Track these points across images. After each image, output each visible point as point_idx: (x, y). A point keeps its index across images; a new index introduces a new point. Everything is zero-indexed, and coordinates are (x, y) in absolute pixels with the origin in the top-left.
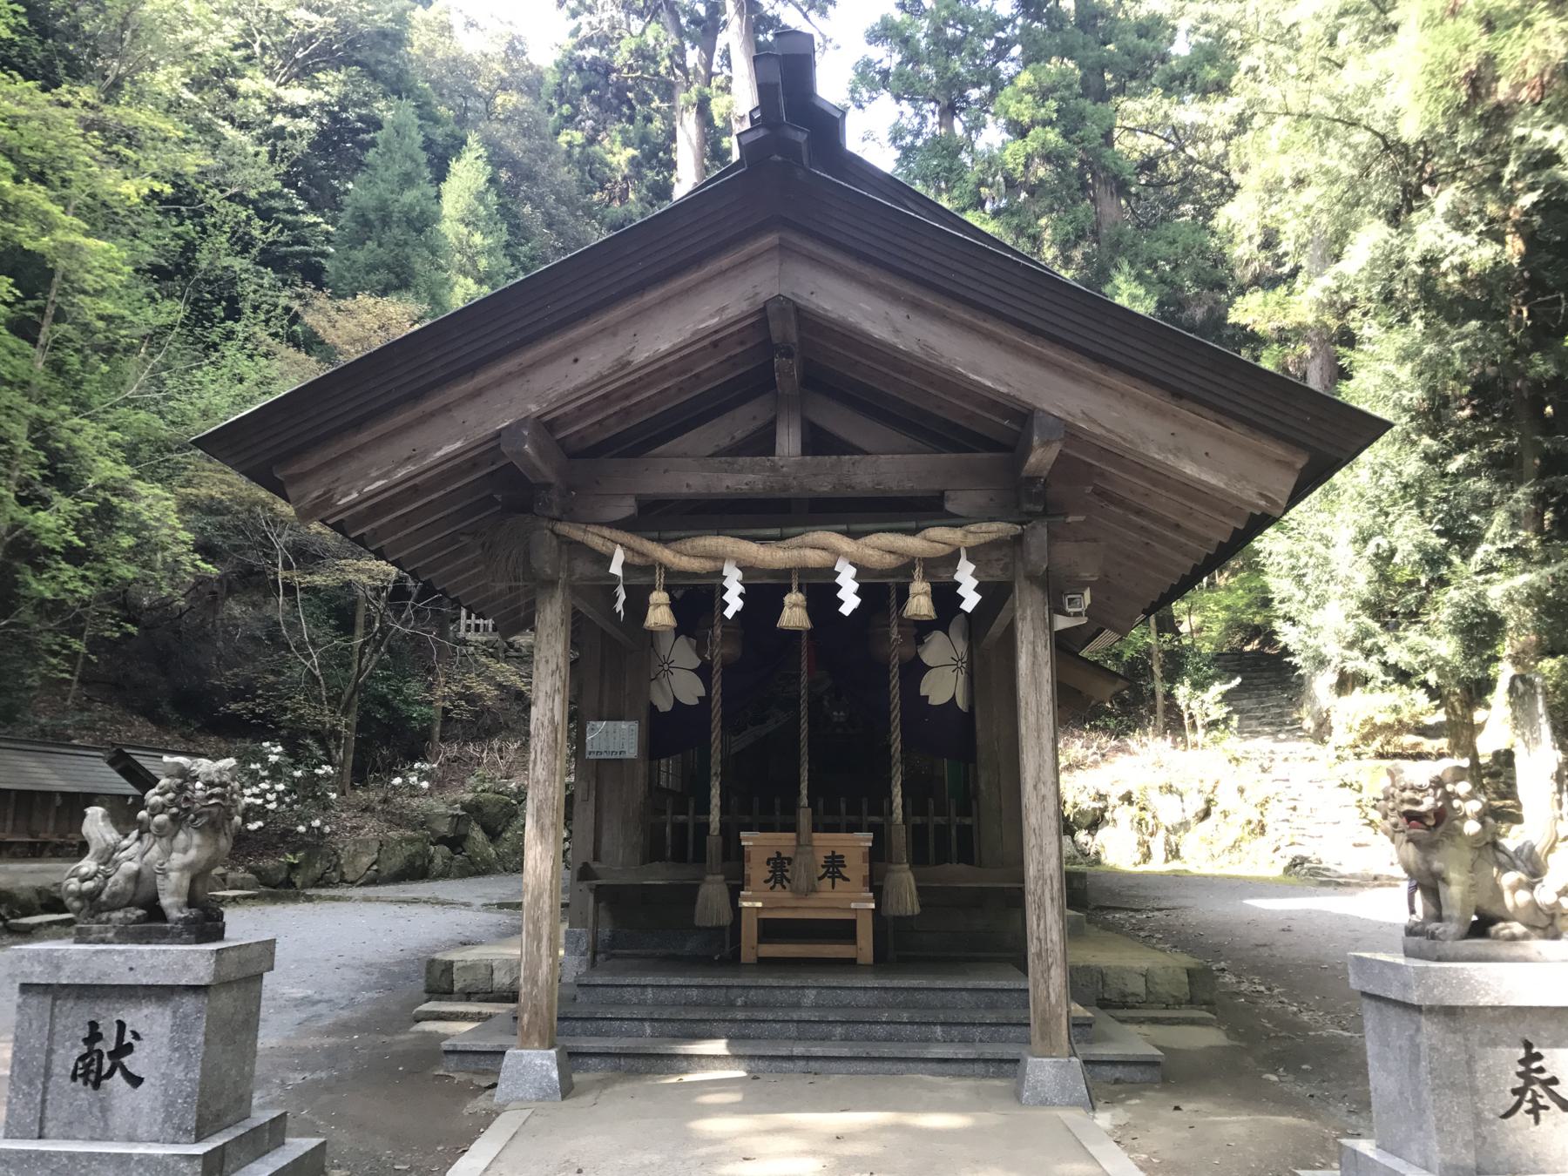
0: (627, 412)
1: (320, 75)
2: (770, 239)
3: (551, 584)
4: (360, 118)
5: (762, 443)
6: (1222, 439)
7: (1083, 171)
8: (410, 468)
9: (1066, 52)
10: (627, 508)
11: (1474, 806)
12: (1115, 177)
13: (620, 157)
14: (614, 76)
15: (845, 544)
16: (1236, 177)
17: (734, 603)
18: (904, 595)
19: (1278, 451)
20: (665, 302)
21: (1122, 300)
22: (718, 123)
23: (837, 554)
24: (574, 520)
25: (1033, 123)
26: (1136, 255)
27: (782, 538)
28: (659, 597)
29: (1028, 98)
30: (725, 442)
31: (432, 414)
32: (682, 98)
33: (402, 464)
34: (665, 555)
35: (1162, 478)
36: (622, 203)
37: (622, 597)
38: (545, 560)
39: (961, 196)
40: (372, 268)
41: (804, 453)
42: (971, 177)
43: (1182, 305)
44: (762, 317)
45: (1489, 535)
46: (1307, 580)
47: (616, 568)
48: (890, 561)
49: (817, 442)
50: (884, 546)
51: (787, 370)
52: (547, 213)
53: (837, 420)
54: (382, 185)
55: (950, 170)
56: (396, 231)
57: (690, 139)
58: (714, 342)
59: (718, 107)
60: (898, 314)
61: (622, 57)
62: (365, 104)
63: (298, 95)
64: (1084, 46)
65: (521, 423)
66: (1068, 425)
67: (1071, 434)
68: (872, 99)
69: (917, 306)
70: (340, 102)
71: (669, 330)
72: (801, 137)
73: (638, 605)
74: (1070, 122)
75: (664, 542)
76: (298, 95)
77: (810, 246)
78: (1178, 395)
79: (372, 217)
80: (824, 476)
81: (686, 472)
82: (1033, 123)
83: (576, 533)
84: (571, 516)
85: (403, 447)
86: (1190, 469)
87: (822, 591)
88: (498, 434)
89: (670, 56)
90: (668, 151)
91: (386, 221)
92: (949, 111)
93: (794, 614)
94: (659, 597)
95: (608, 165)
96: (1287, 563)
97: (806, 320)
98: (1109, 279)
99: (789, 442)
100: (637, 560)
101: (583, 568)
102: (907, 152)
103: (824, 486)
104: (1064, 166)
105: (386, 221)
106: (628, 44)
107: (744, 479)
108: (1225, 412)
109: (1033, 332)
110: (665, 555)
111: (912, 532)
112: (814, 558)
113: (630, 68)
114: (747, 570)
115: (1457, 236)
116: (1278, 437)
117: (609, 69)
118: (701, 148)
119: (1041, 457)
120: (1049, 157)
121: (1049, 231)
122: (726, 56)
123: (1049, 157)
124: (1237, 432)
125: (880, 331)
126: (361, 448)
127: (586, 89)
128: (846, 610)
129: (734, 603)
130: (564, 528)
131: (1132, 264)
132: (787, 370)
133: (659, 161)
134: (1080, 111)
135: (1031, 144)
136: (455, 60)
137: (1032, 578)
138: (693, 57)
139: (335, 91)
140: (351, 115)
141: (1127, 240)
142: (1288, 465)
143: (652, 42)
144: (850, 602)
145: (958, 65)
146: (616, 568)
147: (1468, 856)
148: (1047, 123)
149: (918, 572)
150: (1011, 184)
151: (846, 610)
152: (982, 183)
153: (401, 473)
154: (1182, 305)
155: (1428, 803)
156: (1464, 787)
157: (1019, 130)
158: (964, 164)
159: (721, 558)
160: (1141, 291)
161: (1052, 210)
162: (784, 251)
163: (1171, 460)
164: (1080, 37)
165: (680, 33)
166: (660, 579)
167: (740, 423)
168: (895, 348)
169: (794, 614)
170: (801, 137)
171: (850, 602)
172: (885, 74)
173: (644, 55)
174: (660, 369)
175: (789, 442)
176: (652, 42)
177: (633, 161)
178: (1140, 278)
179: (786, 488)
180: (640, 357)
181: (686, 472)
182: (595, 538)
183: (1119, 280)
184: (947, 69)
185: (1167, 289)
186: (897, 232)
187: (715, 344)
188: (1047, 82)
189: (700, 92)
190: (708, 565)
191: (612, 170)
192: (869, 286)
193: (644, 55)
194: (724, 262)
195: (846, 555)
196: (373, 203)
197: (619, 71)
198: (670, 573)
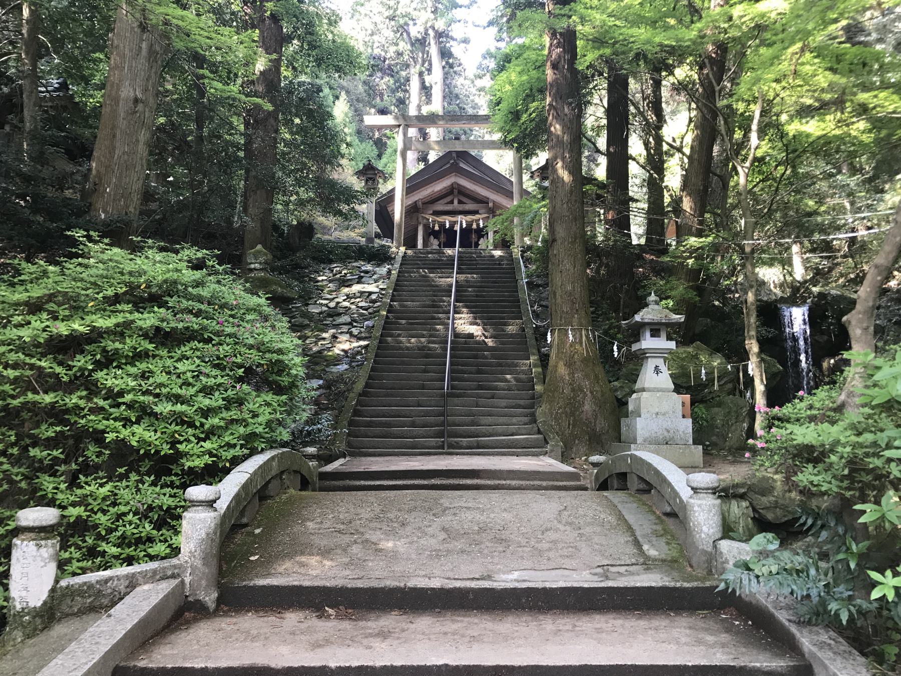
5: (452, 202)
17: (447, 226)
38: (420, 219)
49: (460, 202)
50: (470, 218)
51: (456, 191)
53: (464, 199)
67: (494, 202)
71: (440, 186)
73: (434, 227)
75: (268, 575)
80: (461, 207)
81: (440, 207)
99: (456, 202)
103: (461, 209)
107: (449, 208)
119: (491, 205)
121: (688, 61)
129: (447, 226)
132: (456, 191)
167: (449, 199)
175: (456, 202)
179: (810, 632)
180: (436, 190)
181: (440, 207)
182: (427, 216)
196: (818, 444)
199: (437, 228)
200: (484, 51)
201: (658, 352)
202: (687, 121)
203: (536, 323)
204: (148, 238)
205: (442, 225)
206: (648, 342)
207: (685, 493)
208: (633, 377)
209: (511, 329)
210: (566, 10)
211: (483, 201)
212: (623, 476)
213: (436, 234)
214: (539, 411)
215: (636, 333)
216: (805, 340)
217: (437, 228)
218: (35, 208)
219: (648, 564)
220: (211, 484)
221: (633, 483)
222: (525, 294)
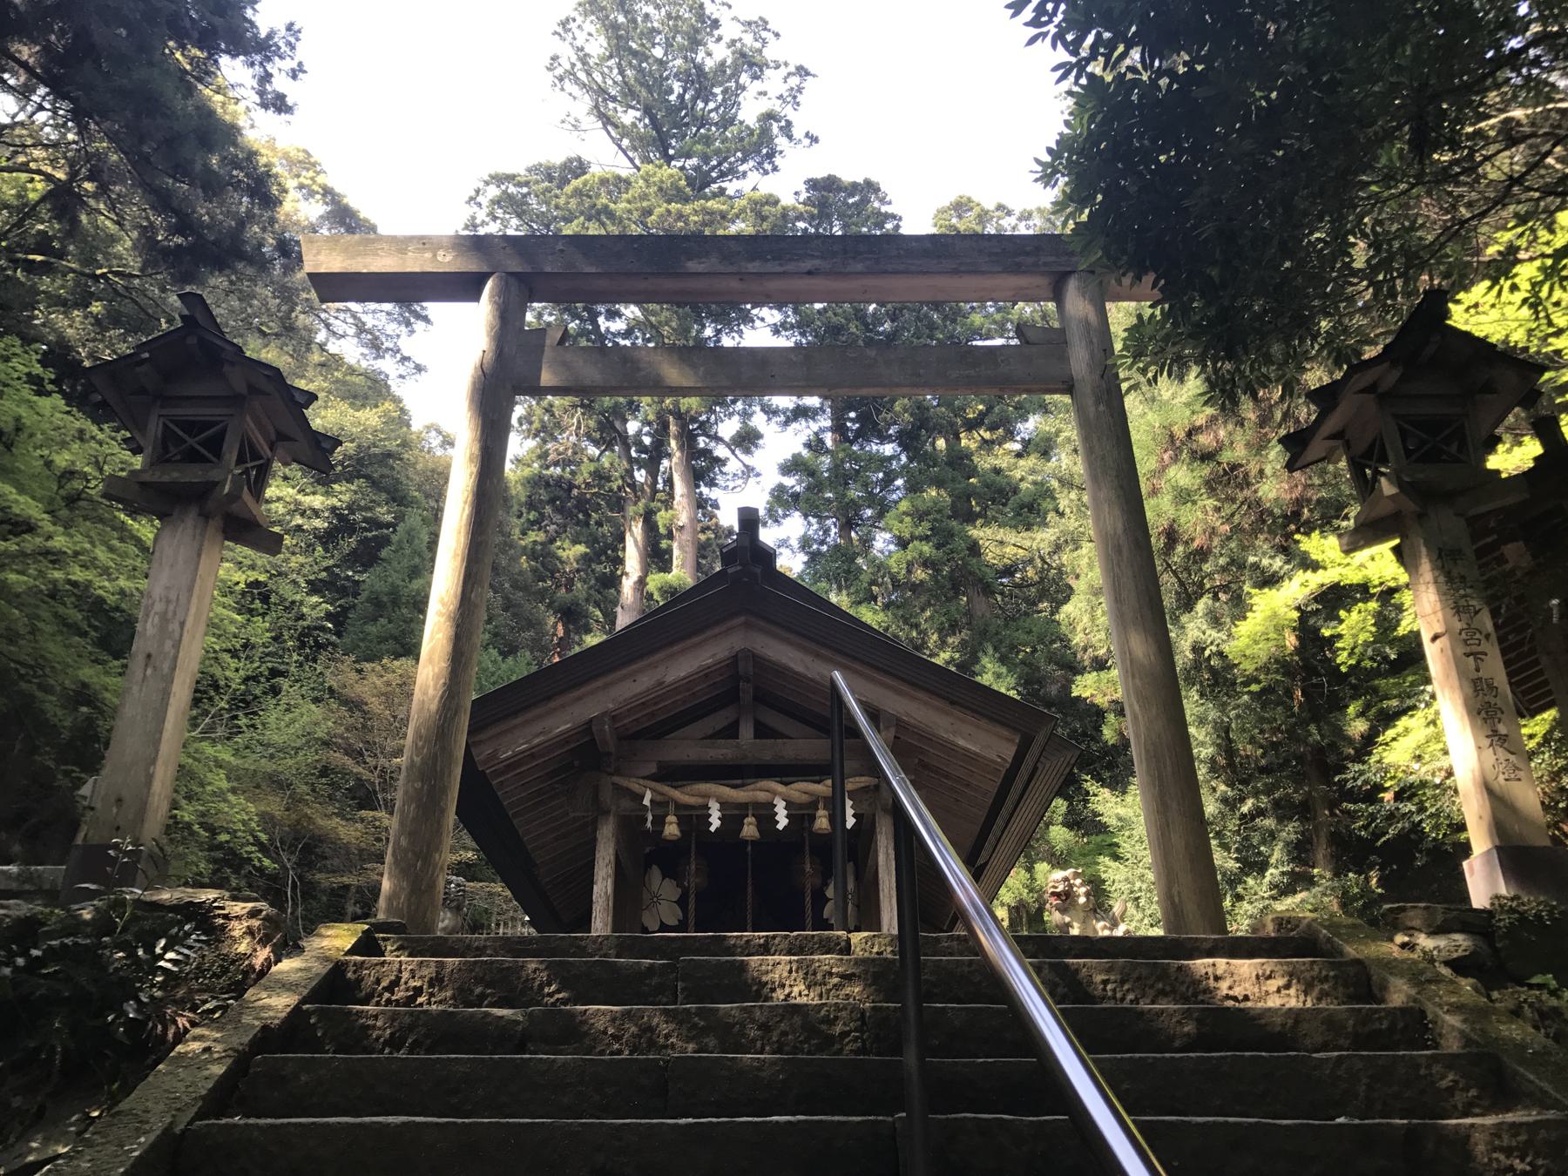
0: (653, 714)
1: (336, 487)
2: (742, 619)
3: (607, 813)
4: (365, 520)
5: (731, 732)
6: (978, 727)
7: (959, 578)
8: (542, 738)
9: (939, 483)
10: (652, 769)
11: (1083, 890)
12: (981, 580)
13: (571, 552)
14: (575, 492)
15: (780, 788)
16: (1072, 582)
17: (715, 823)
18: (813, 818)
19: (1005, 732)
20: (682, 651)
21: (986, 679)
22: (662, 531)
23: (775, 793)
24: (620, 775)
25: (913, 538)
26: (1001, 641)
27: (743, 785)
28: (671, 818)
29: (908, 519)
30: (710, 732)
31: (555, 709)
32: (631, 510)
33: (538, 735)
34: (676, 794)
35: (950, 749)
36: (569, 590)
37: (650, 818)
38: (607, 796)
39: (857, 592)
40: (382, 640)
41: (756, 737)
42: (865, 578)
43: (1041, 682)
44: (735, 660)
45: (1273, 861)
46: (1142, 902)
47: (646, 802)
48: (805, 798)
49: (762, 731)
50: (802, 789)
52: (506, 598)
54: (395, 575)
55: (848, 572)
56: (404, 611)
57: (636, 541)
58: (705, 674)
59: (662, 518)
60: (808, 659)
61: (584, 474)
62: (370, 509)
63: (317, 501)
64: (953, 480)
65: (604, 714)
66: (898, 719)
68: (785, 516)
69: (818, 655)
70: (349, 507)
71: (683, 666)
72: (758, 571)
73: (660, 821)
74: (941, 537)
76: (317, 501)
77: (762, 623)
78: (953, 703)
79: (385, 599)
80: (768, 751)
81: (686, 748)
82: (913, 538)
83: (624, 782)
84: (618, 772)
85: (537, 727)
86: (961, 742)
87: (765, 814)
88: (591, 720)
89: (622, 477)
90: (615, 550)
91: (396, 603)
92: (847, 525)
93: (749, 830)
94: (671, 818)
95: (559, 559)
96: (1125, 887)
97: (758, 661)
98: (977, 661)
99: (747, 732)
100: (659, 798)
101: (626, 804)
102: (814, 557)
104: (937, 571)
105: (396, 603)
106: (586, 469)
107: (721, 752)
108: (977, 712)
109: (877, 669)
110: (676, 794)
111: (819, 782)
112: (762, 796)
113: (587, 484)
114: (724, 806)
115: (1214, 634)
116: (1003, 724)
117: (571, 486)
118: (645, 549)
120: (926, 563)
122: (669, 482)
123: (926, 563)
124: (983, 723)
125: (799, 668)
126: (515, 727)
127: (552, 501)
128: (780, 827)
129: (715, 823)
130: (616, 779)
131: (996, 649)
133: (608, 557)
134: (944, 530)
135: (910, 554)
136: (433, 471)
137: (885, 810)
138: (640, 476)
139: (346, 498)
140: (358, 517)
141: (992, 629)
142: (1012, 741)
143: (607, 465)
144: (782, 822)
145: (855, 493)
146: (646, 802)
147: (1082, 915)
148: (926, 538)
149: (821, 805)
150: (896, 584)
151: (780, 827)
152: (873, 583)
153: (536, 741)
154: (1041, 682)
155: (1060, 888)
156: (1078, 881)
157: (902, 543)
158: (860, 569)
159: (707, 796)
160: (1004, 670)
161: (930, 605)
162: (748, 626)
163: (952, 738)
164: (950, 473)
165: (631, 460)
166: (672, 808)
167: (719, 720)
168: (805, 677)
169: (749, 830)
170: (758, 571)
171: (782, 822)
172: (796, 496)
173: (600, 476)
174: (688, 683)
175: (747, 732)
176: (607, 465)
177: (585, 558)
178: (1003, 660)
180: (670, 679)
181: (686, 748)
182: (635, 786)
183: (985, 661)
184: (844, 495)
185: (1027, 669)
186: (792, 608)
187: (706, 675)
188: (922, 507)
189: (646, 506)
190: (700, 801)
191: (562, 562)
192: (790, 643)
193: (600, 476)
194: (717, 630)
195: (780, 794)
197: (579, 487)
198: (679, 806)
200: (1455, 770)
202: (353, 201)
205: (694, 819)
210: (1348, 560)
213: (669, 858)
217: (672, 829)
218: (722, 191)
220: (300, 253)
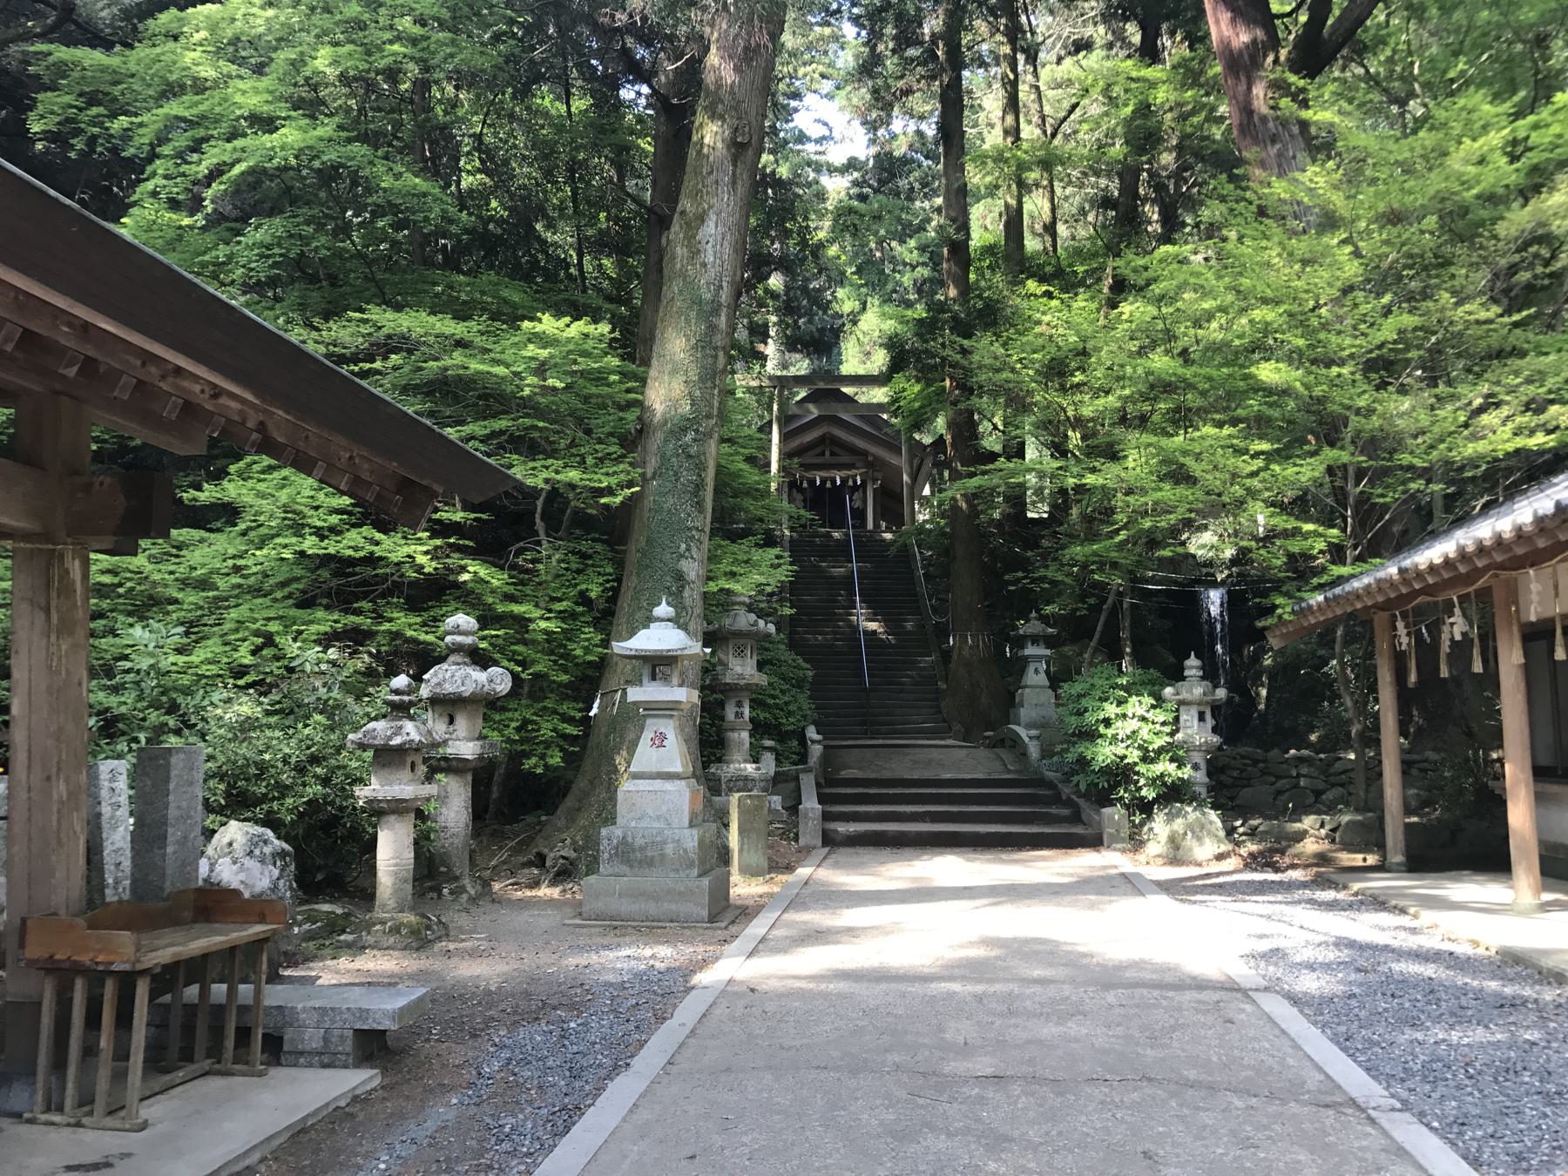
49: (833, 454)
50: (844, 473)
53: (837, 450)
80: (834, 460)
99: (827, 453)
107: (819, 460)
167: (819, 450)
175: (827, 453)
199: (805, 485)
201: (1039, 658)
203: (935, 619)
204: (1297, 815)
205: (812, 482)
206: (1030, 650)
207: (1026, 740)
208: (1022, 672)
209: (909, 625)
211: (865, 453)
212: (1003, 740)
214: (943, 704)
215: (1020, 642)
216: (1223, 623)
219: (1009, 771)
221: (1008, 742)
222: (923, 587)
